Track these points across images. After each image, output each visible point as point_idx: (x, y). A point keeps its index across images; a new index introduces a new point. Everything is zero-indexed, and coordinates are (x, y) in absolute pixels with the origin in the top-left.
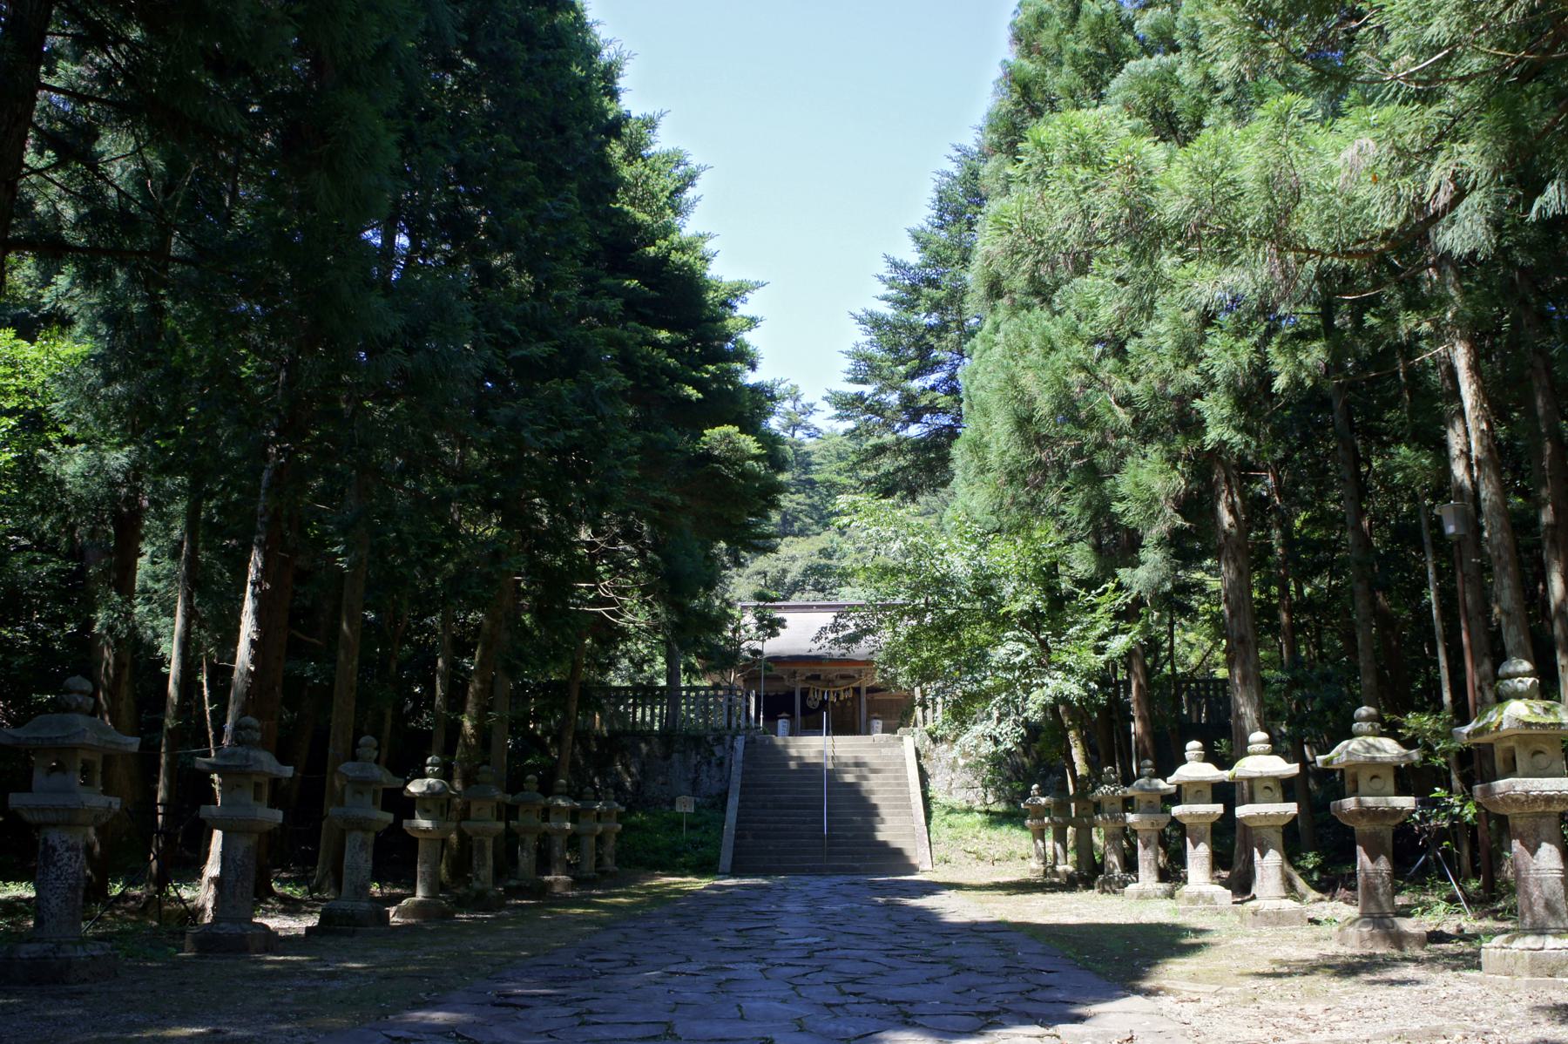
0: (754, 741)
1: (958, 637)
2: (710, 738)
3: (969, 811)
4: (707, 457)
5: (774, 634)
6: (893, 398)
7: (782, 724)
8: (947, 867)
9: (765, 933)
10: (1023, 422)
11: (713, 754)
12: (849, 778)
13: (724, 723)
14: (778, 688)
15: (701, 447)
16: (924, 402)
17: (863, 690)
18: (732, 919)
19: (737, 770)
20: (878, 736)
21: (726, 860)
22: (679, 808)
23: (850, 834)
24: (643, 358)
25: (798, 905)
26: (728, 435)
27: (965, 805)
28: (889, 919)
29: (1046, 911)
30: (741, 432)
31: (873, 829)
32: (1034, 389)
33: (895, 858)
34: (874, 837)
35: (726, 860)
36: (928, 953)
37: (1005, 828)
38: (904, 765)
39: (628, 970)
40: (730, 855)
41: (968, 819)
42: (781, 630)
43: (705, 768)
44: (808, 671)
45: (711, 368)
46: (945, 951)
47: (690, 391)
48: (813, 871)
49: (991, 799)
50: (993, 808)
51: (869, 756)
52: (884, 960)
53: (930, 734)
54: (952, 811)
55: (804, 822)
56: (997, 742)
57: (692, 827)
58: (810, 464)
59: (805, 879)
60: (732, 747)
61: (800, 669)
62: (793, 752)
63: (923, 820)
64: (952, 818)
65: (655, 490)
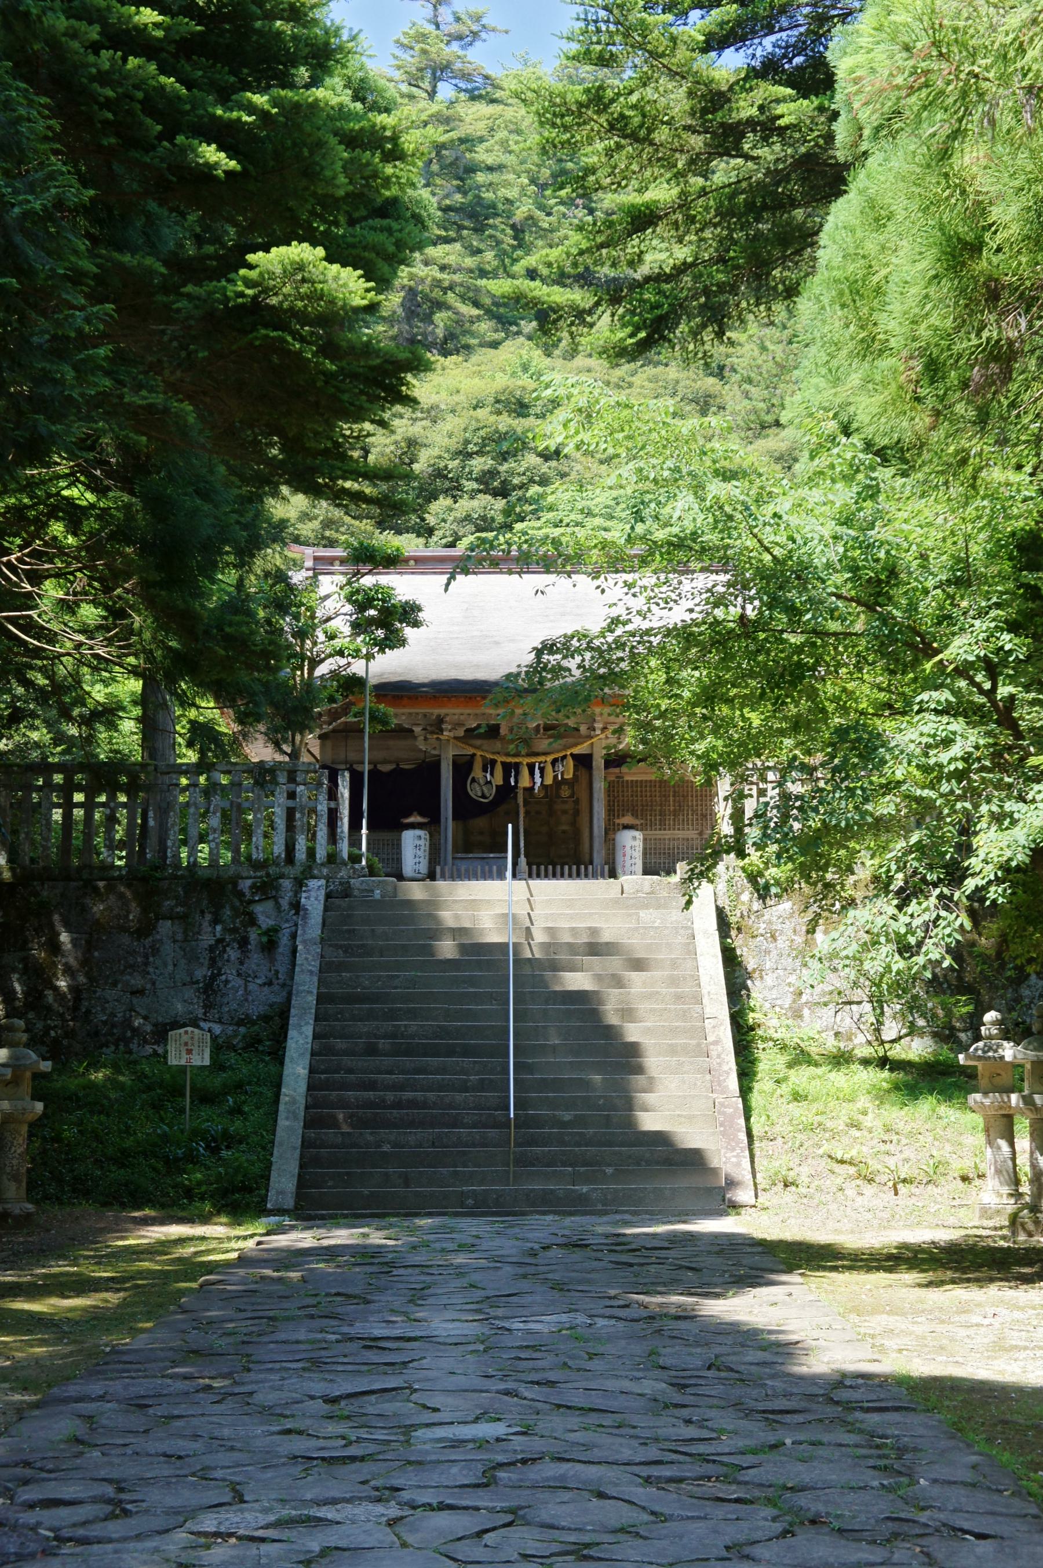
0: (346, 892)
1: (812, 694)
2: (245, 885)
3: (840, 1060)
4: (256, 312)
5: (393, 641)
6: (675, 99)
7: (413, 846)
8: (789, 1196)
9: (389, 1407)
10: (960, 251)
11: (253, 921)
12: (577, 981)
13: (279, 849)
14: (402, 754)
15: (239, 287)
16: (745, 109)
17: (599, 762)
18: (316, 1364)
19: (308, 959)
20: (633, 880)
21: (283, 1182)
22: (175, 1059)
23: (567, 1116)
24: (103, 78)
25: (456, 1298)
26: (300, 267)
27: (831, 1044)
28: (652, 1362)
29: (1000, 1347)
30: (330, 259)
31: (629, 1105)
32: (985, 184)
33: (678, 1169)
34: (630, 1123)
35: (283, 1182)
36: (732, 1474)
37: (927, 1105)
38: (691, 950)
39: (115, 1528)
40: (294, 1167)
41: (839, 1079)
42: (409, 632)
43: (233, 954)
44: (469, 716)
45: (260, 100)
46: (771, 1471)
47: (211, 154)
48: (482, 1206)
49: (891, 1030)
50: (897, 1052)
51: (612, 928)
52: (641, 1493)
53: (753, 878)
54: (801, 1057)
55: (464, 1088)
56: (905, 950)
57: (205, 1098)
58: (471, 169)
59: (471, 1227)
60: (296, 906)
61: (452, 712)
62: (448, 917)
63: (733, 1083)
64: (801, 1077)
65: (138, 387)
